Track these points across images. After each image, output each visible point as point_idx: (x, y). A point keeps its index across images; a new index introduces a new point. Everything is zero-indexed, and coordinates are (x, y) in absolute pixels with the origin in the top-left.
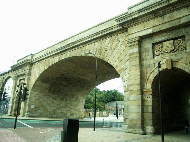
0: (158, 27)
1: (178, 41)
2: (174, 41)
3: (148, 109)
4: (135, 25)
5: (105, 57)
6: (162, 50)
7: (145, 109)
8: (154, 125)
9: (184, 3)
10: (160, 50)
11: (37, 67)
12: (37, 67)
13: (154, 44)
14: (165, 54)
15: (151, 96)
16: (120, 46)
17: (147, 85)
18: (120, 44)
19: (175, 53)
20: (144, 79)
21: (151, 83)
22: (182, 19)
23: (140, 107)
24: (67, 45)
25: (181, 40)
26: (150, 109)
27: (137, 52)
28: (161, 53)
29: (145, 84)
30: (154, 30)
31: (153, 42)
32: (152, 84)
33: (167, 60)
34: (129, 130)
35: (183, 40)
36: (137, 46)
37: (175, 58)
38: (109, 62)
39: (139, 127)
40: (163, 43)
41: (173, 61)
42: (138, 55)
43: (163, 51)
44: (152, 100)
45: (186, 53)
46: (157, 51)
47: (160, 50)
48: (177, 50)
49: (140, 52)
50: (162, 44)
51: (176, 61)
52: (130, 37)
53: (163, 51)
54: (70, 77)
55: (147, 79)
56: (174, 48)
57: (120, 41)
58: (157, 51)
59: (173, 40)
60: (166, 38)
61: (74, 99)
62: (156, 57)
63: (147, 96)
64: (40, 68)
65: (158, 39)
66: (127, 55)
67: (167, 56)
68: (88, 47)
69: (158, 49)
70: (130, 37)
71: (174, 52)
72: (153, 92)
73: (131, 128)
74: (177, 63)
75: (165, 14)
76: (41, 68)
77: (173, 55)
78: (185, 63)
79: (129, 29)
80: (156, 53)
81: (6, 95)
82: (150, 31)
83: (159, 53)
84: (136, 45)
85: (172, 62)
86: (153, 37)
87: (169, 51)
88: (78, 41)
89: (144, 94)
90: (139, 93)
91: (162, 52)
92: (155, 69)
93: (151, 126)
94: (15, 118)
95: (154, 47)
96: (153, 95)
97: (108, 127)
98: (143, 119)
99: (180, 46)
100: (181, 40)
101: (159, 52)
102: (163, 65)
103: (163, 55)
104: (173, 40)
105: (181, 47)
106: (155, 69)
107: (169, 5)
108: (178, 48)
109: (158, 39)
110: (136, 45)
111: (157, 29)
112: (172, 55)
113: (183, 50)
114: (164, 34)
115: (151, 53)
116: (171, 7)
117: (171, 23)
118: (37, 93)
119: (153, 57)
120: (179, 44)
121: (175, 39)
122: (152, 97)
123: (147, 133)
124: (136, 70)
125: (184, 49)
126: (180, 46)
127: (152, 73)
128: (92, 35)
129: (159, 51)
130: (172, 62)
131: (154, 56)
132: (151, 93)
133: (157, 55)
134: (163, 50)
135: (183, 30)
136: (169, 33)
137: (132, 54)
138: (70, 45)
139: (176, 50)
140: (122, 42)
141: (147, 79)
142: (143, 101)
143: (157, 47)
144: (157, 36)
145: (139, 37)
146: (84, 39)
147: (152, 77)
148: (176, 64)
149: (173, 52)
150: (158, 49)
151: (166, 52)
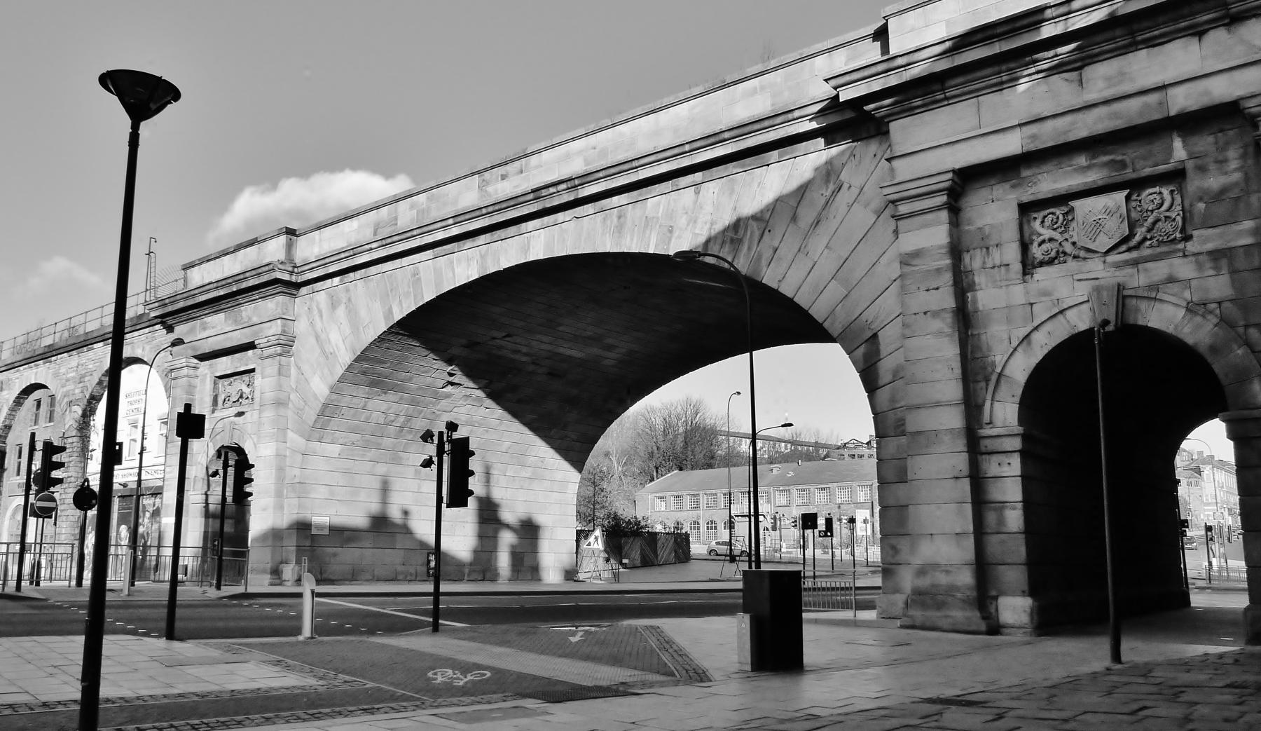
0: (1049, 124)
1: (1149, 196)
2: (1128, 198)
3: (1001, 521)
4: (927, 107)
5: (764, 262)
6: (1066, 236)
7: (991, 518)
8: (1034, 589)
9: (1184, 17)
10: (1056, 235)
11: (334, 306)
12: (334, 306)
13: (1026, 209)
14: (1085, 259)
15: (1016, 461)
16: (843, 209)
17: (996, 404)
18: (844, 197)
19: (1134, 254)
20: (980, 377)
21: (1017, 399)
22: (1172, 92)
23: (968, 508)
24: (534, 191)
25: (1166, 192)
26: (1014, 519)
27: (940, 247)
28: (1065, 253)
29: (988, 404)
30: (1034, 137)
31: (1026, 198)
32: (1022, 404)
33: (1098, 290)
34: (918, 614)
35: (1172, 192)
36: (944, 215)
37: (1136, 280)
38: (787, 290)
39: (966, 602)
40: (1076, 204)
41: (1126, 293)
42: (947, 261)
43: (1074, 244)
44: (1025, 477)
45: (1190, 258)
46: (1043, 242)
47: (1056, 235)
48: (1145, 239)
49: (956, 251)
50: (1065, 209)
51: (1140, 294)
52: (904, 169)
53: (1074, 244)
54: (517, 357)
55: (994, 378)
56: (1132, 226)
57: (846, 186)
58: (1043, 242)
59: (1125, 192)
60: (1094, 177)
61: (527, 473)
62: (1041, 274)
63: (995, 459)
64: (352, 312)
65: (1049, 182)
66: (884, 260)
67: (1095, 267)
68: (657, 202)
69: (1047, 233)
70: (904, 169)
71: (1129, 250)
72: (1025, 437)
73: (924, 606)
74: (1143, 305)
75: (1087, 61)
76: (363, 313)
77: (1127, 263)
78: (1184, 304)
79: (895, 127)
80: (1037, 252)
81: (55, 458)
82: (1011, 145)
83: (1053, 254)
84: (938, 209)
85: (1122, 296)
86: (1025, 173)
87: (1104, 243)
88: (601, 175)
89: (983, 449)
90: (961, 444)
91: (1068, 248)
92: (1036, 328)
93: (1023, 594)
94: (429, 588)
95: (1025, 220)
96: (1024, 453)
97: (827, 611)
98: (983, 566)
99: (1157, 221)
100: (1166, 192)
101: (1054, 245)
102: (1075, 310)
103: (1071, 264)
104: (1125, 192)
105: (1166, 227)
106: (1036, 328)
107: (1112, 23)
108: (1149, 230)
109: (1049, 182)
110: (938, 209)
111: (1049, 134)
112: (1119, 266)
113: (1175, 239)
114: (1082, 160)
115: (1012, 253)
116: (1118, 32)
117: (1116, 107)
118: (335, 449)
119: (1025, 274)
120: (1152, 211)
121: (1135, 186)
122: (1023, 463)
123: (1004, 627)
124: (939, 333)
125: (1178, 235)
126: (1157, 221)
127: (1020, 349)
128: (687, 148)
129: (1051, 240)
130: (1122, 296)
131: (1028, 266)
132: (1016, 443)
133: (1042, 264)
134: (1075, 239)
135: (1178, 144)
136: (1106, 154)
137: (917, 254)
138: (552, 190)
139: (1138, 238)
140: (855, 191)
141: (994, 378)
142: (978, 481)
143: (1043, 222)
144: (1045, 168)
145: (954, 171)
146: (635, 164)
147: (1020, 369)
148: (1137, 310)
149: (1124, 248)
150: (1047, 233)
151: (1089, 250)
